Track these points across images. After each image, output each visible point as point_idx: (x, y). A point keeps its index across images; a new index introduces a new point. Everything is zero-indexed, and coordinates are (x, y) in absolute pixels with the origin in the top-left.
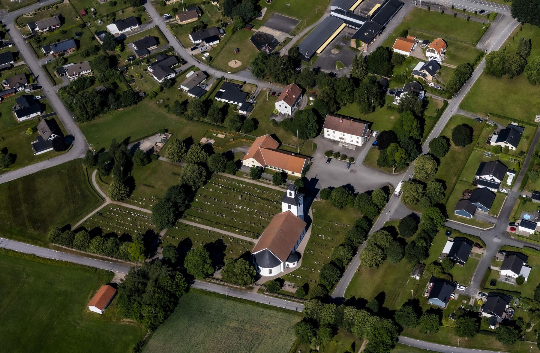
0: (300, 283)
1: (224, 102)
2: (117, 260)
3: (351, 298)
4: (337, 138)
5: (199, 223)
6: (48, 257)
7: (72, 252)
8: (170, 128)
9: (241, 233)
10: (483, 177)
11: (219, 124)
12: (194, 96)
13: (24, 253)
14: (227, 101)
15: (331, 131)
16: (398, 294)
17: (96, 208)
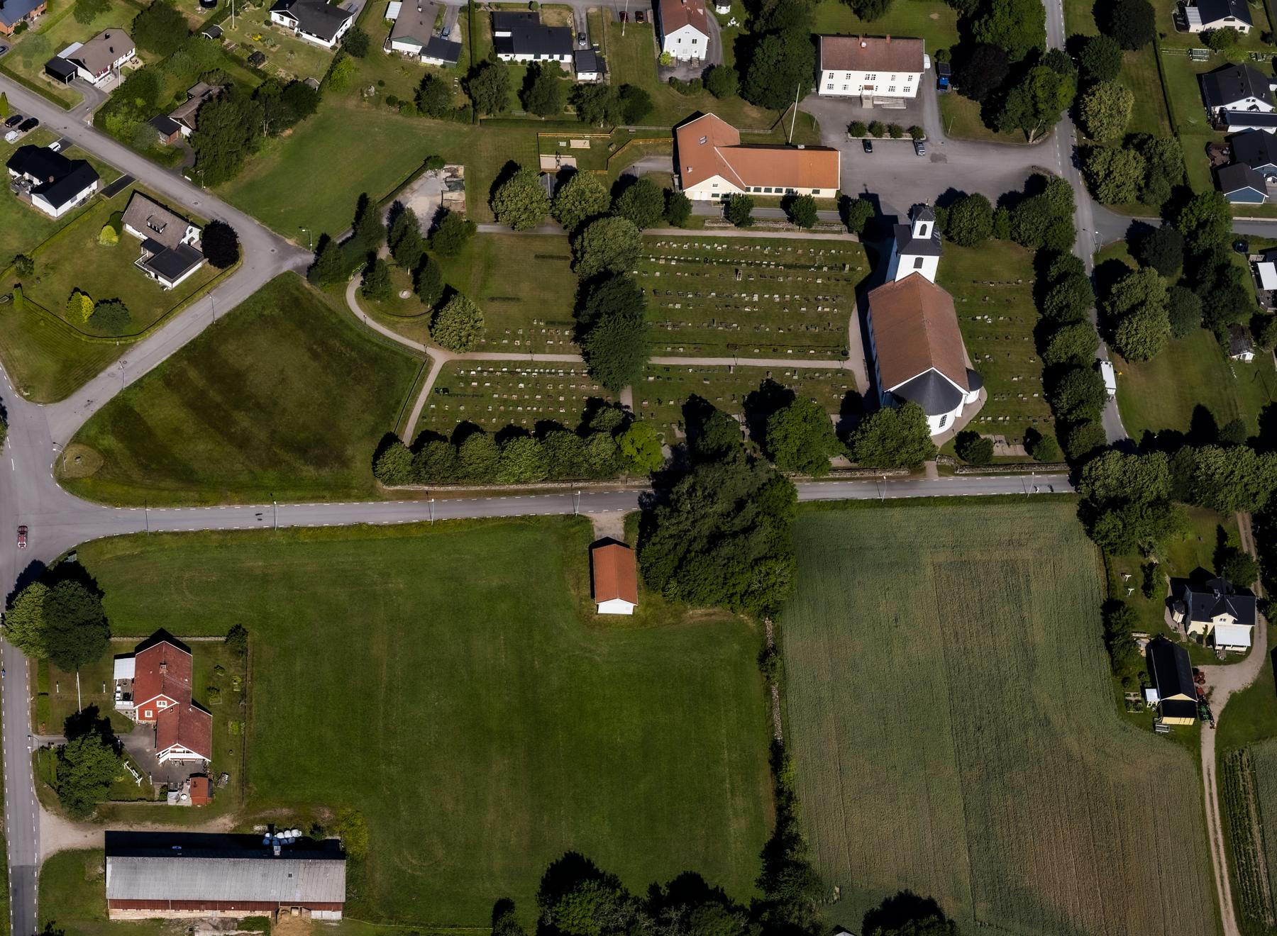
0: (1015, 433)
1: (524, 62)
2: (569, 485)
3: (1144, 435)
4: (853, 91)
5: (691, 356)
6: (400, 522)
7: (439, 495)
8: (442, 152)
9: (802, 353)
10: (1229, 107)
11: (499, 115)
12: (440, 62)
13: (377, 526)
14: (530, 57)
15: (840, 75)
16: (1233, 403)
17: (423, 380)
